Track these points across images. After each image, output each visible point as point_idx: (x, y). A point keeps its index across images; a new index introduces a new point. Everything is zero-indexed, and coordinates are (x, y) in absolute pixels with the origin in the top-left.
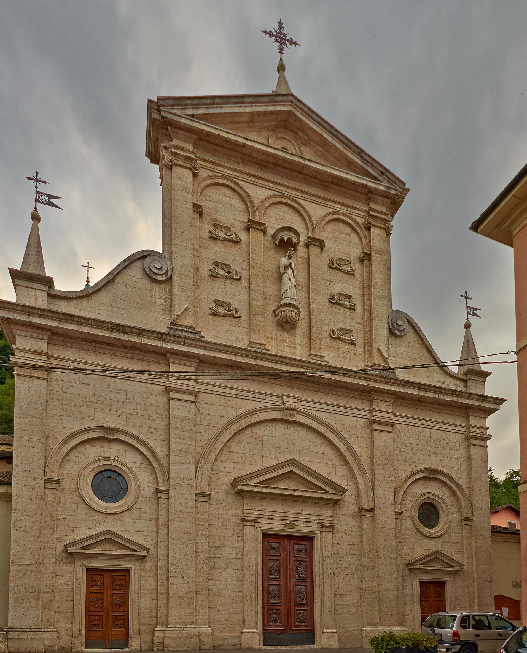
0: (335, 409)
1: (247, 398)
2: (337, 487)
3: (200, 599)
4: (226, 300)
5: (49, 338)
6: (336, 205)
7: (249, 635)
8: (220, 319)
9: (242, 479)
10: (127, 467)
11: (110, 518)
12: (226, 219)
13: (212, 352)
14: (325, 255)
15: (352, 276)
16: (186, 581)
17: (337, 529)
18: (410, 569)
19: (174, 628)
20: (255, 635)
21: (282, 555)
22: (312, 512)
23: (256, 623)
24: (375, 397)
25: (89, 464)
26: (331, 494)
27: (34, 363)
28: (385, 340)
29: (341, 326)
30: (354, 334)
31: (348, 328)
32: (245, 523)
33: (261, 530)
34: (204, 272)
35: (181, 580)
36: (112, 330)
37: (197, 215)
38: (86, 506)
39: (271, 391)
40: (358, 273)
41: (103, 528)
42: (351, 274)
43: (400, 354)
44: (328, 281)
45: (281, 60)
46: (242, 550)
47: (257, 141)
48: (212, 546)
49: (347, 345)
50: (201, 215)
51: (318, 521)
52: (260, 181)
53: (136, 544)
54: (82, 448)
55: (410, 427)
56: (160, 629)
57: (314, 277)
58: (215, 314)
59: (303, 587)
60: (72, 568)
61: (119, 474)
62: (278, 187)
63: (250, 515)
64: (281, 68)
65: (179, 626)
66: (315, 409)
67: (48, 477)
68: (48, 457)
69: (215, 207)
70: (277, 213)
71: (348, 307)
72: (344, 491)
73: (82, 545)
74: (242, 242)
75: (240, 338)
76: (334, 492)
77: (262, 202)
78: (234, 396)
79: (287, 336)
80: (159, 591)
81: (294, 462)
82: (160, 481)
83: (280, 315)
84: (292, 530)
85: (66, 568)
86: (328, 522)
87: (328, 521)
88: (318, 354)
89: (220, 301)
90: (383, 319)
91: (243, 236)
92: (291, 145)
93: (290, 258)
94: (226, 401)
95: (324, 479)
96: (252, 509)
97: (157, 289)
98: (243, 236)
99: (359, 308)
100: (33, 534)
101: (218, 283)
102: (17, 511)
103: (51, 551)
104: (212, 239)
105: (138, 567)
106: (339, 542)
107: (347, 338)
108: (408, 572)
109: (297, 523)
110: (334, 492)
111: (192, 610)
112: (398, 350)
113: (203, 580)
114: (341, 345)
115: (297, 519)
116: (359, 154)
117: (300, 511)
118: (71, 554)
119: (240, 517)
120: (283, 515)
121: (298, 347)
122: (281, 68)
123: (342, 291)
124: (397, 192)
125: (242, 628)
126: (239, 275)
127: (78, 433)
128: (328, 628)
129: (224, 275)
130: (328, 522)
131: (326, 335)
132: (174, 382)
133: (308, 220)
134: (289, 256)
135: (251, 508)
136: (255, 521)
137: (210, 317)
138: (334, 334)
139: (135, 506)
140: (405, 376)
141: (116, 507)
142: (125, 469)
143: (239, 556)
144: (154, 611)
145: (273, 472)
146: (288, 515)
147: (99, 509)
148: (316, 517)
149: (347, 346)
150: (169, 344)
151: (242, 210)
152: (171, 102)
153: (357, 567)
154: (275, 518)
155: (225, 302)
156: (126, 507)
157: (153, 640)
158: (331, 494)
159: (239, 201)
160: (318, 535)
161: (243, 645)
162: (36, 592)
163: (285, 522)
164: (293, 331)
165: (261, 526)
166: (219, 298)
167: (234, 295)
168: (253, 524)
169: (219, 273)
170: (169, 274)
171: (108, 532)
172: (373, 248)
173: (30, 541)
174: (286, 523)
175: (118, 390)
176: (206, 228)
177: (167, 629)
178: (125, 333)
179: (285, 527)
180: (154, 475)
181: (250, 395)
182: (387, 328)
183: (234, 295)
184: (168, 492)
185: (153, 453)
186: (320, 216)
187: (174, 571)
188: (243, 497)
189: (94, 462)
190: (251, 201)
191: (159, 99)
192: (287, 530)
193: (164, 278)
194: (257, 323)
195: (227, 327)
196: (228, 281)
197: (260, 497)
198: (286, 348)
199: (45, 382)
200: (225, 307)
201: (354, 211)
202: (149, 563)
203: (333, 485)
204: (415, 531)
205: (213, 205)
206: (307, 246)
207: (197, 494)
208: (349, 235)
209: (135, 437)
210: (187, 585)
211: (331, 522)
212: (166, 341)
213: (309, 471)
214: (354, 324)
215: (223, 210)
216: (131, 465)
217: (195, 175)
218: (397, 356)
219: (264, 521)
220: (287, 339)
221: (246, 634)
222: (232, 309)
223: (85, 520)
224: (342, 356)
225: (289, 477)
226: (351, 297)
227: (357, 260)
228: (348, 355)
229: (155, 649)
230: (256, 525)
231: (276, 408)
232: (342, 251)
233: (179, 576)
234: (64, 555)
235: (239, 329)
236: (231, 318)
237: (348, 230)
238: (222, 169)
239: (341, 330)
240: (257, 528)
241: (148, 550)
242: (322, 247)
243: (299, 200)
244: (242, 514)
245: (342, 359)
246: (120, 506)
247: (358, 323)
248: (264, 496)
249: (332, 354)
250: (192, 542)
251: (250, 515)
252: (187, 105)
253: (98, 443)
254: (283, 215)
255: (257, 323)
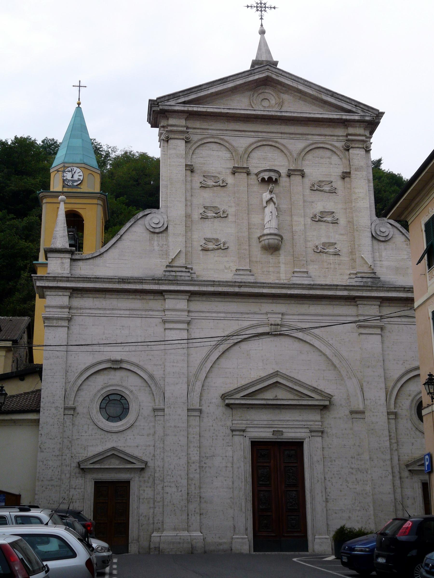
0: (321, 318)
1: (234, 319)
2: (323, 393)
3: (192, 507)
4: (215, 236)
5: (71, 293)
6: (314, 137)
7: (240, 540)
8: (209, 253)
9: (229, 393)
10: (129, 390)
11: (115, 436)
12: (214, 169)
13: (201, 287)
14: (306, 180)
15: (334, 194)
16: (180, 490)
17: (327, 433)
18: (410, 471)
19: (168, 534)
20: (244, 541)
21: (272, 461)
22: (300, 418)
23: (246, 529)
24: (361, 302)
25: (99, 391)
26: (317, 400)
27: (60, 316)
28: (370, 248)
29: (324, 240)
30: (338, 246)
31: (332, 241)
32: (234, 433)
33: (250, 438)
34: (196, 216)
35: (174, 489)
36: (119, 282)
37: (189, 172)
38: (96, 427)
39: (256, 310)
40: (340, 190)
41: (109, 445)
42: (333, 191)
43: (387, 257)
44: (310, 202)
45: (262, 25)
46: (231, 459)
47: (240, 105)
48: (204, 456)
49: (331, 256)
50: (192, 171)
51: (306, 426)
52: (243, 133)
53: (136, 458)
54: (92, 379)
55: (400, 326)
56: (156, 535)
57: (296, 202)
58: (205, 250)
59: (295, 492)
60: (83, 481)
61: (122, 396)
62: (260, 134)
63: (238, 425)
64: (262, 32)
65: (173, 532)
66: (300, 321)
67: (66, 405)
68: (67, 389)
69: (204, 162)
70: (259, 154)
71: (330, 222)
72: (330, 396)
73: (91, 462)
74: (229, 185)
75: (227, 266)
76: (320, 398)
77: (246, 150)
78: (223, 318)
79: (271, 257)
80: (155, 499)
81: (279, 373)
82: (157, 401)
83: (263, 242)
84: (279, 437)
85: (79, 481)
86: (317, 427)
87: (316, 426)
88: (301, 270)
89: (209, 239)
90: (366, 229)
91: (230, 180)
92: (271, 96)
93: (271, 192)
94: (217, 321)
95: (309, 387)
96: (242, 419)
97: (156, 239)
98: (230, 180)
99: (342, 221)
100: (54, 454)
101: (208, 223)
102: (43, 435)
103: (67, 467)
104: (202, 188)
105: (137, 479)
106: (330, 446)
107: (331, 250)
108: (406, 474)
109: (284, 430)
110: (320, 398)
111: (185, 517)
112: (384, 254)
113: (199, 489)
114: (325, 257)
115: (285, 426)
116: (332, 96)
117: (287, 418)
118: (83, 469)
119: (229, 428)
120: (271, 423)
121: (282, 266)
122: (262, 32)
123: (324, 208)
124: (372, 117)
125: (233, 534)
126: (227, 213)
127: (91, 367)
128: (320, 534)
129: (213, 216)
130: (317, 427)
131: (310, 251)
132: (169, 315)
133: (288, 154)
134: (270, 191)
135: (239, 418)
136: (244, 431)
137: (201, 252)
138: (318, 249)
139: (136, 424)
140: (392, 277)
141: (120, 426)
142: (127, 392)
143: (229, 465)
144: (151, 519)
145: (259, 384)
146: (276, 423)
147: (106, 429)
148: (304, 423)
149: (332, 257)
150: (164, 286)
151: (229, 158)
152: (167, 98)
153: (351, 470)
154: (263, 425)
155: (214, 239)
156: (128, 425)
157: (150, 545)
158: (317, 400)
159: (225, 152)
160: (306, 440)
161: (233, 551)
162: (55, 503)
163: (272, 430)
164: (277, 252)
165: (248, 435)
166: (209, 236)
167: (224, 231)
168: (242, 433)
169: (209, 215)
170: (165, 226)
171: (113, 449)
172: (353, 167)
173: (52, 460)
174: (274, 431)
175: (123, 326)
176: (198, 179)
177: (162, 535)
178: (129, 283)
179: (273, 434)
180: (151, 395)
181: (238, 316)
182: (371, 236)
183: (224, 231)
184: (163, 410)
185: (151, 377)
186: (300, 149)
187: (169, 481)
188: (232, 409)
189: (102, 389)
190: (236, 151)
191: (158, 99)
192: (275, 437)
193: (162, 230)
194: (243, 251)
195: (216, 258)
196: (216, 220)
197: (248, 408)
198: (271, 268)
199: (67, 328)
200: (214, 242)
201: (333, 138)
202: (147, 474)
203: (319, 391)
204: (414, 429)
205: (203, 160)
206: (289, 176)
207: (188, 410)
208: (329, 158)
209: (136, 365)
210: (180, 493)
211: (320, 427)
212: (162, 284)
213: (294, 380)
214: (337, 236)
215: (212, 162)
216: (132, 388)
217: (187, 142)
218: (383, 259)
219: (252, 430)
220: (271, 261)
221: (236, 540)
222: (220, 243)
223: (94, 438)
224: (326, 267)
225: (276, 386)
226: (333, 212)
227: (339, 178)
228: (332, 266)
229: (151, 553)
230: (245, 434)
231: (262, 325)
232: (323, 173)
233: (173, 485)
234: (77, 470)
235: (226, 259)
236: (219, 250)
237: (328, 153)
238: (210, 131)
239: (324, 244)
240: (245, 436)
241: (146, 463)
242: (303, 176)
243: (279, 140)
244: (231, 425)
245: (327, 270)
246: (123, 425)
247: (341, 235)
248: (251, 406)
249: (315, 266)
250: (184, 454)
251: (238, 425)
252: (180, 96)
253: (105, 372)
254: (265, 154)
255: (243, 251)
